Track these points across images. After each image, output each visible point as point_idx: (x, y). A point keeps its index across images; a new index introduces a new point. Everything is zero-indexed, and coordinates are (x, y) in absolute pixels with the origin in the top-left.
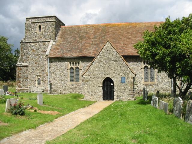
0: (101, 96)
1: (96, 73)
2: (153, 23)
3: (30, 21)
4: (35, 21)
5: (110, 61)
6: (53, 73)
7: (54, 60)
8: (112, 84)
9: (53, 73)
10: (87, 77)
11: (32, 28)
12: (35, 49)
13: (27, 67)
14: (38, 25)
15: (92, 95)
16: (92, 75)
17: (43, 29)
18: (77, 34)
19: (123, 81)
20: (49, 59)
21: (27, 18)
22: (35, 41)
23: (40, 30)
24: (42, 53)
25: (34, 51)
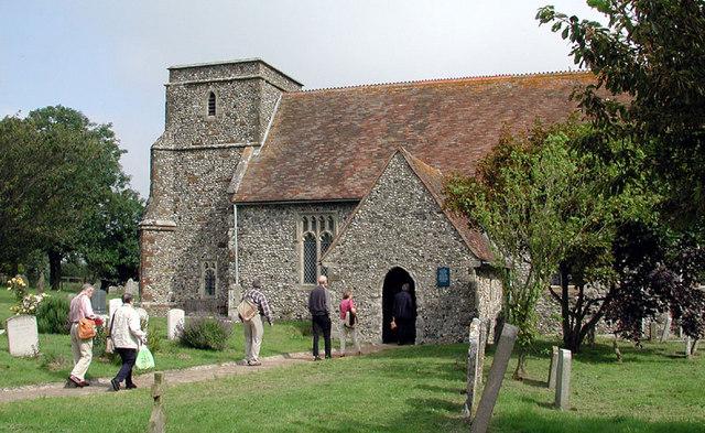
0: (377, 327)
3: (183, 80)
4: (197, 78)
5: (404, 215)
11: (188, 102)
14: (205, 92)
17: (221, 104)
18: (334, 121)
19: (443, 279)
20: (238, 207)
21: (171, 70)
23: (212, 111)
25: (194, 180)
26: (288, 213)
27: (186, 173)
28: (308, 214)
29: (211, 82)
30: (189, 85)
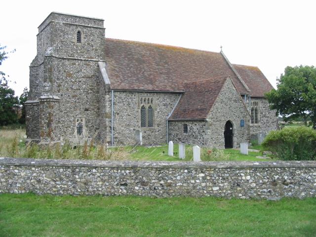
1: (218, 115)
2: (149, 46)
6: (118, 114)
7: (119, 93)
8: (231, 129)
9: (118, 114)
10: (210, 120)
12: (71, 72)
13: (59, 102)
15: (215, 143)
16: (215, 117)
17: (84, 38)
22: (71, 58)
23: (79, 40)
24: (84, 80)
25: (70, 75)
26: (135, 96)
27: (65, 71)
28: (143, 96)
29: (79, 25)
30: (66, 24)
